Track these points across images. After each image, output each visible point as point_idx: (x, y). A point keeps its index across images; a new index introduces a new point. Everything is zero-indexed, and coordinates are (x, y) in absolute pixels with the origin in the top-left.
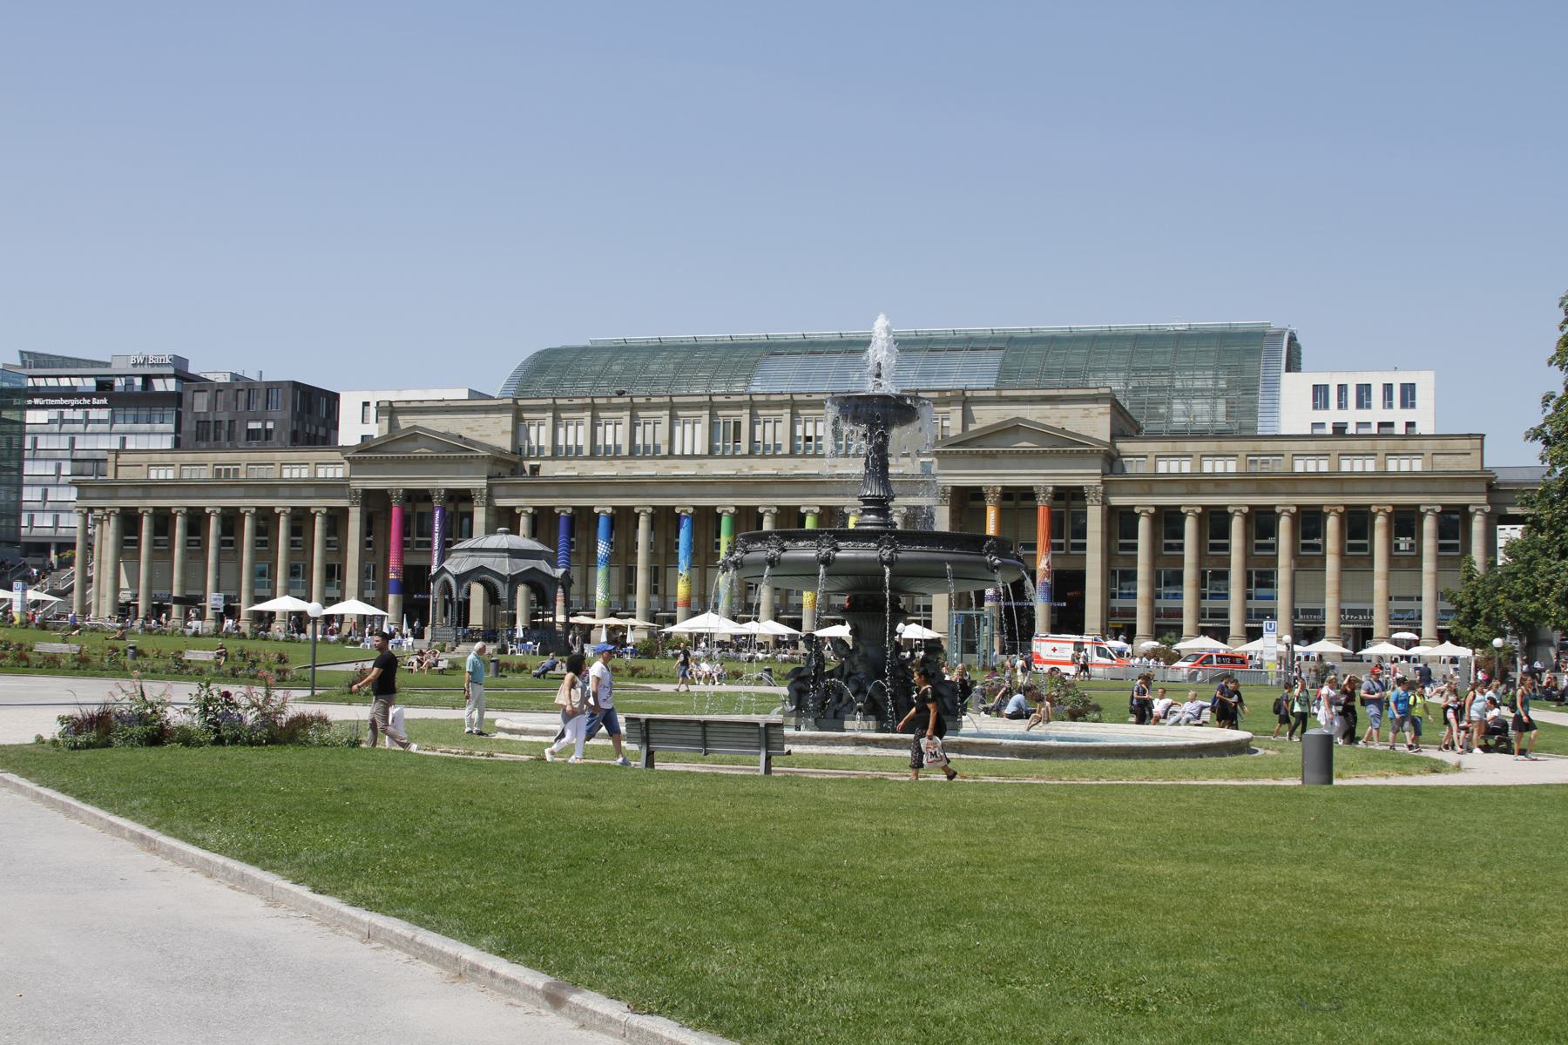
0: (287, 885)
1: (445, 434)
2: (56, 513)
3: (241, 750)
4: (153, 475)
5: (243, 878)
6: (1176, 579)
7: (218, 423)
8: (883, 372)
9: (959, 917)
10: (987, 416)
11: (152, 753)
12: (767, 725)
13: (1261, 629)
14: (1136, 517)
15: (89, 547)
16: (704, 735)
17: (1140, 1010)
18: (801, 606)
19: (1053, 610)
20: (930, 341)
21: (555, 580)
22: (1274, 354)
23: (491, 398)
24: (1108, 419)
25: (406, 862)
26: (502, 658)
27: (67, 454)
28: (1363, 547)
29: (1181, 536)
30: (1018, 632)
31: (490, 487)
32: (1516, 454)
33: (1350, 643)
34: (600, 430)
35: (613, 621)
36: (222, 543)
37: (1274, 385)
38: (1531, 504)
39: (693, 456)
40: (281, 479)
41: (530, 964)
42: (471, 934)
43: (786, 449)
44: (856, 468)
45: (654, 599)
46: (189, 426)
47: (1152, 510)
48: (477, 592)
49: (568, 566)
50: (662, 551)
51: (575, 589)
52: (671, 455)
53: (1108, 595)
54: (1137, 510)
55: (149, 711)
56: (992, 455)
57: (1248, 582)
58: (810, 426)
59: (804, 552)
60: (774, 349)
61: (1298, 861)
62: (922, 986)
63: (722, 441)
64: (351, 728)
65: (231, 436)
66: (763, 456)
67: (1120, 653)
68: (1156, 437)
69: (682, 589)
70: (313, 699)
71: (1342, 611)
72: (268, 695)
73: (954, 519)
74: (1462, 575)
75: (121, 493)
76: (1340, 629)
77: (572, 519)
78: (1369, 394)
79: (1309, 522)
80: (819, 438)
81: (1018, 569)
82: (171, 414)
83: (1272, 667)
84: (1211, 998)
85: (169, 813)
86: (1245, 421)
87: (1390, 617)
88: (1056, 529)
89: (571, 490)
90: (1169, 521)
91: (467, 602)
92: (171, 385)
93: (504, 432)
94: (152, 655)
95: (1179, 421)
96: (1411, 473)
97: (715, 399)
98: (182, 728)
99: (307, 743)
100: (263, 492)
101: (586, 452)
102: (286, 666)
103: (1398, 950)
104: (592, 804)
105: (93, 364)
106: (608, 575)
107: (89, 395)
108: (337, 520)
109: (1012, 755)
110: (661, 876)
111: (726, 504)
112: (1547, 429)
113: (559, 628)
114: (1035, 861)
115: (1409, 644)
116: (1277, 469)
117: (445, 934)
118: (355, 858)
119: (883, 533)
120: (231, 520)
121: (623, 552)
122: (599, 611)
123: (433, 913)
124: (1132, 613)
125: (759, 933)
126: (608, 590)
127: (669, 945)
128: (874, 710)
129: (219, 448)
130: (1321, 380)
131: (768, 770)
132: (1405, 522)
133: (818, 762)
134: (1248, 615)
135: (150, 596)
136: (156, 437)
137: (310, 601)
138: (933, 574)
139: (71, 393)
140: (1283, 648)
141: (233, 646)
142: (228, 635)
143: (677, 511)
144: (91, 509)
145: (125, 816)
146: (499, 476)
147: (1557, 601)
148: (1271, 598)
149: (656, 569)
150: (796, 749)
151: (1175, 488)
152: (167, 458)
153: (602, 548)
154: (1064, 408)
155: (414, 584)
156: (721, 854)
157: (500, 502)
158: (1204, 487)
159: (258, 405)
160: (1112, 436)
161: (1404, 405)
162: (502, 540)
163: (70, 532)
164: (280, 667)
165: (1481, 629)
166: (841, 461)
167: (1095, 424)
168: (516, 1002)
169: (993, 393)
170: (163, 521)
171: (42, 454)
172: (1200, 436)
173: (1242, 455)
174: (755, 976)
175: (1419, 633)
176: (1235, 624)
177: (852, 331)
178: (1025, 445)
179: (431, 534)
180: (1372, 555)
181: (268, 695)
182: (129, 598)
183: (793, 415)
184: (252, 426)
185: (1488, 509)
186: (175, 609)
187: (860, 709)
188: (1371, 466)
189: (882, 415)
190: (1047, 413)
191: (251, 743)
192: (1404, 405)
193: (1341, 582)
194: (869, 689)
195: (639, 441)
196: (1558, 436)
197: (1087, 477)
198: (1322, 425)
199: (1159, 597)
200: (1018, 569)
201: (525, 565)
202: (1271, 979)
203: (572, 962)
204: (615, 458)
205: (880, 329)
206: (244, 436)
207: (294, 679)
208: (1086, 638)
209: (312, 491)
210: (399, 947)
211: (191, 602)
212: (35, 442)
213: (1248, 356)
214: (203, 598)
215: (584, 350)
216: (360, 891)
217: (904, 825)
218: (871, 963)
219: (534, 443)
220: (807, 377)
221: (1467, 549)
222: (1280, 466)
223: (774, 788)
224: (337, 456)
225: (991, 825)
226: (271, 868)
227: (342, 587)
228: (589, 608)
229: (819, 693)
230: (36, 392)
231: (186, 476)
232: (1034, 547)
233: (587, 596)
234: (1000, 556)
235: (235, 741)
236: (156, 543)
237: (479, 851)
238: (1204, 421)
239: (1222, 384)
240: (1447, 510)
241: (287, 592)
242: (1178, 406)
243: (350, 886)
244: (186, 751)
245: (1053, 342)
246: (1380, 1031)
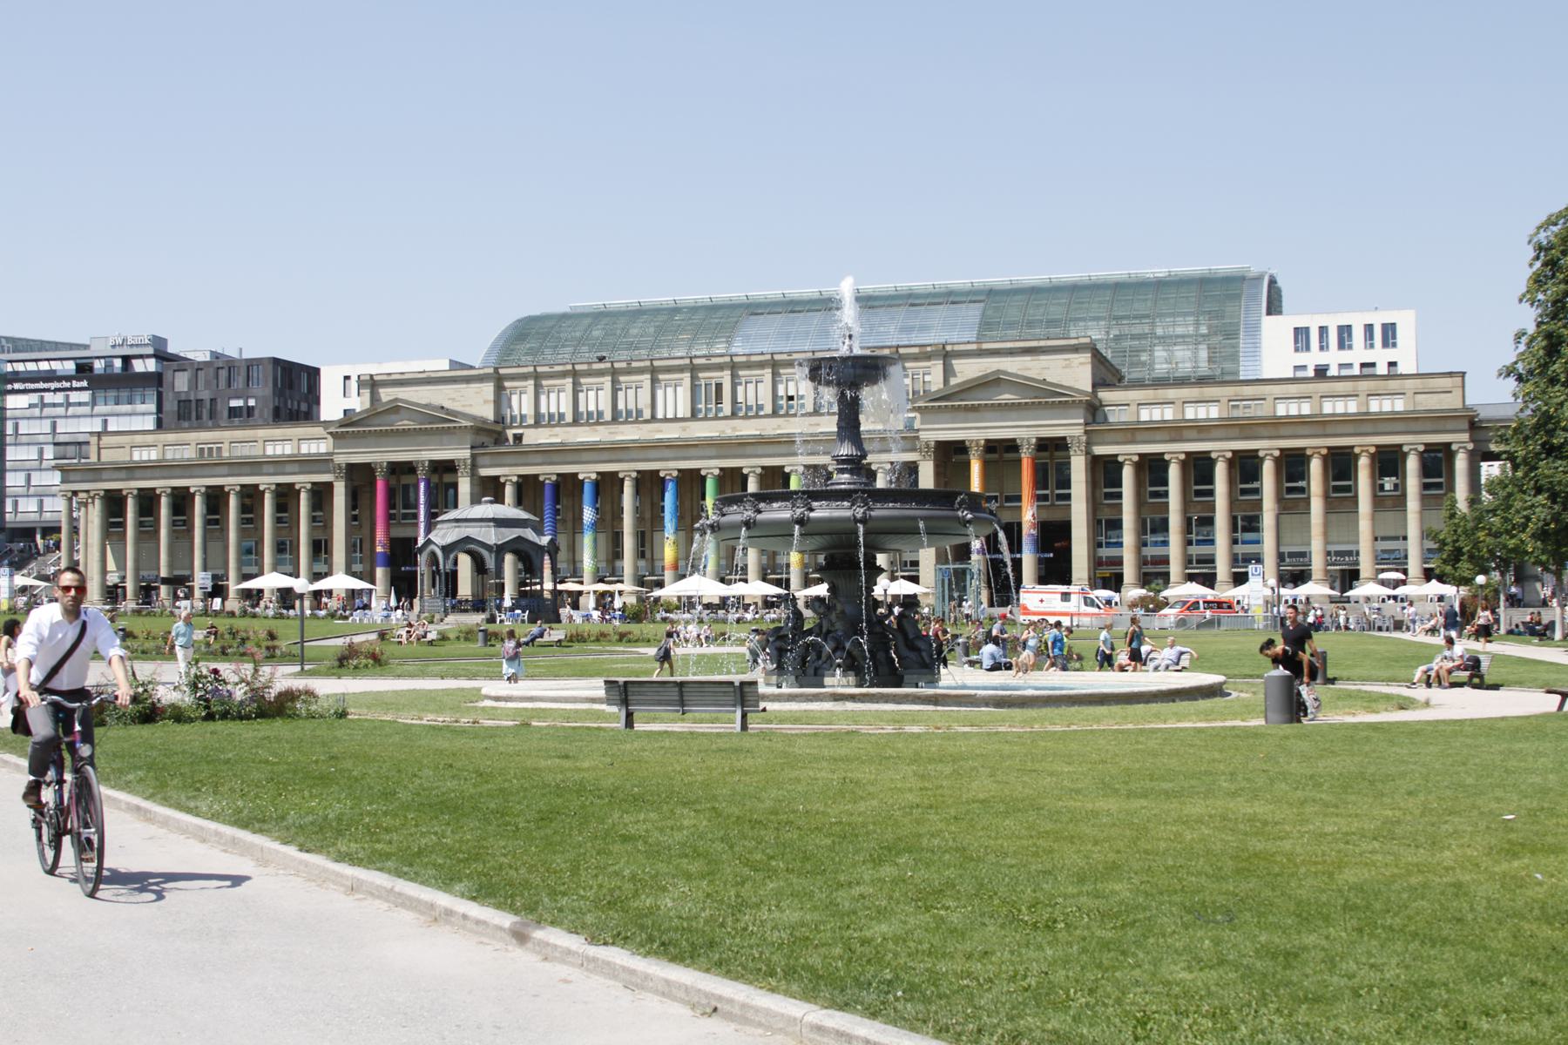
0: (276, 846)
1: (426, 406)
2: (41, 497)
3: (231, 724)
4: (136, 457)
5: (234, 841)
6: (1162, 526)
7: (199, 401)
8: (849, 334)
9: (898, 854)
10: (967, 370)
11: (145, 731)
12: (742, 683)
13: (1246, 574)
14: (1120, 466)
15: (75, 530)
16: (682, 695)
17: (1050, 926)
18: (788, 566)
19: (1040, 561)
20: (910, 296)
21: (541, 547)
22: (1255, 297)
23: (472, 368)
24: (1088, 368)
25: (387, 821)
26: (491, 628)
27: (50, 438)
28: (1347, 489)
29: (1166, 483)
30: (1003, 588)
31: (473, 457)
32: (1495, 395)
33: (1337, 584)
34: (582, 396)
35: (602, 587)
36: (207, 522)
37: (1255, 329)
38: (1506, 441)
39: (676, 420)
40: (265, 456)
41: (498, 906)
42: (446, 881)
43: (768, 409)
44: (829, 425)
45: (642, 563)
46: (170, 406)
47: (1136, 458)
48: (465, 564)
49: (555, 533)
50: (648, 515)
51: (563, 555)
52: (653, 419)
53: (1095, 544)
54: (1120, 459)
55: (140, 690)
56: (974, 409)
57: (1234, 528)
58: (791, 385)
59: (779, 512)
60: (755, 308)
61: (1234, 795)
62: (855, 913)
63: (704, 402)
64: (338, 701)
65: (213, 414)
66: (746, 417)
67: (1109, 602)
68: (1138, 384)
69: (669, 553)
70: (303, 673)
71: (1328, 553)
72: (256, 671)
73: (938, 474)
74: (1445, 513)
75: (105, 475)
76: (1327, 572)
77: (556, 486)
78: (1350, 335)
79: (1293, 465)
80: (802, 397)
81: (991, 522)
82: (152, 394)
83: (1258, 611)
84: (1117, 916)
85: (163, 785)
86: (1228, 366)
87: (1376, 557)
88: (1040, 480)
89: (556, 458)
90: (1152, 469)
91: (454, 574)
92: (151, 365)
93: (486, 402)
94: (142, 636)
95: (1161, 368)
96: (1393, 413)
97: (696, 361)
98: (173, 706)
99: (294, 716)
100: (247, 469)
101: (569, 418)
102: (276, 643)
103: (1303, 870)
104: (567, 764)
105: (72, 346)
106: (595, 540)
107: (68, 378)
108: (321, 495)
109: (987, 705)
110: (626, 825)
111: (711, 467)
112: (1520, 366)
113: (547, 595)
114: (982, 802)
115: (1397, 584)
116: (1259, 414)
117: (422, 883)
118: (339, 819)
119: (856, 491)
120: (216, 499)
121: (608, 517)
122: (587, 576)
123: (411, 865)
124: (1119, 562)
125: (711, 873)
126: (595, 556)
127: (629, 886)
128: (853, 666)
129: (201, 427)
130: (1301, 322)
131: (744, 727)
132: (1388, 462)
133: (795, 718)
134: (1235, 560)
135: (138, 578)
136: (139, 416)
137: (297, 576)
138: (906, 530)
139: (50, 376)
140: (1268, 592)
141: (223, 624)
142: (216, 614)
143: (662, 474)
144: (75, 493)
145: (121, 789)
146: (483, 446)
147: (1533, 536)
148: (1258, 542)
149: (643, 533)
150: (770, 706)
151: (1158, 436)
152: (150, 438)
153: (588, 515)
154: (1045, 359)
155: (402, 556)
156: (684, 804)
157: (484, 472)
158: (1186, 434)
159: (239, 383)
160: (1094, 386)
161: (1385, 344)
162: (488, 510)
163: (54, 517)
164: (270, 643)
165: (1465, 567)
166: (811, 418)
167: (1076, 374)
168: (485, 940)
169: (974, 347)
170: (148, 501)
171: (24, 439)
172: (1182, 382)
173: (1224, 400)
174: (703, 909)
175: (1405, 572)
176: (1222, 569)
177: (828, 290)
178: (1007, 397)
179: (416, 506)
180: (1356, 496)
181: (256, 671)
182: (116, 580)
183: (775, 374)
184: (234, 403)
185: (1470, 446)
186: (164, 589)
187: (839, 666)
188: (1352, 407)
189: (852, 375)
190: (1030, 364)
191: (241, 718)
192: (1385, 344)
193: (1326, 525)
194: (848, 645)
195: (621, 406)
196: (1530, 372)
197: (1070, 427)
198: (1304, 367)
199: (1145, 545)
200: (991, 522)
201: (511, 534)
202: (1177, 898)
203: (537, 903)
204: (598, 423)
205: (846, 289)
206: (226, 413)
207: (284, 656)
208: (1072, 589)
209: (296, 468)
210: (379, 897)
211: (179, 582)
212: (16, 427)
213: (1225, 300)
214: (190, 578)
215: (564, 317)
216: (344, 849)
217: (864, 773)
218: (811, 895)
219: (516, 412)
220: (787, 336)
221: (1451, 488)
222: (1261, 410)
223: (747, 743)
224: (319, 431)
225: (948, 770)
226: (261, 831)
227: (329, 562)
228: (576, 574)
229: (797, 650)
230: (16, 377)
231: (169, 456)
232: (1019, 498)
233: (574, 562)
234: (971, 510)
235: (225, 716)
236: (141, 524)
237: (456, 809)
238: (1185, 368)
239: (1204, 330)
240: (1430, 448)
241: (274, 569)
242: (1160, 353)
243: (334, 844)
244: (178, 727)
245: (1033, 292)
246: (1263, 939)
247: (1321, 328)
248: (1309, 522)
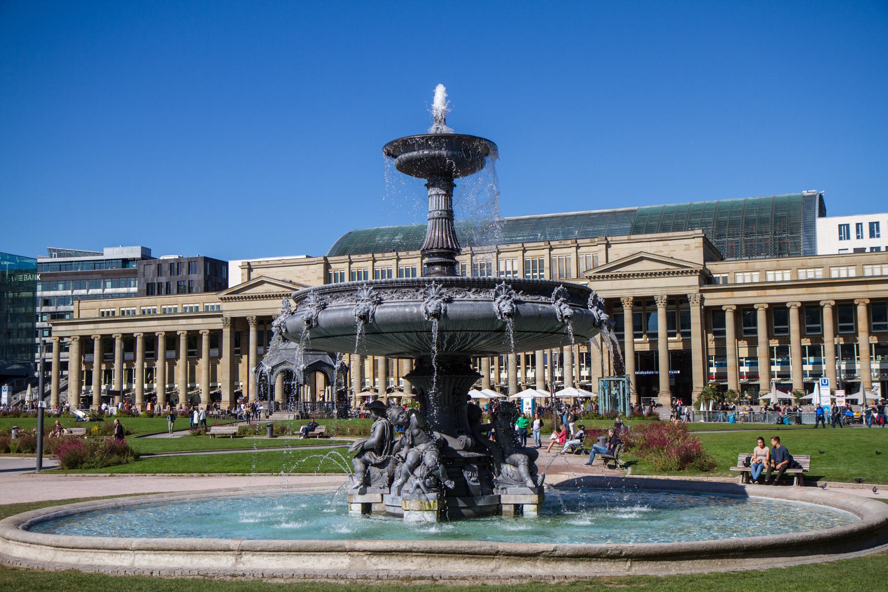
54: (724, 308)
93: (319, 278)
130: (844, 220)
160: (705, 261)
197: (688, 285)
247: (857, 224)
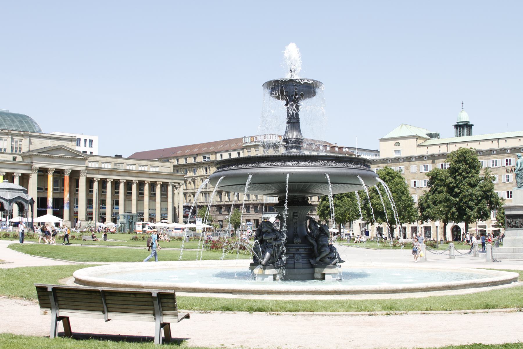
56: (52, 157)
173: (113, 163)
176: (108, 217)
178: (63, 155)
201: (16, 195)
240: (23, 174)
248: (143, 204)
